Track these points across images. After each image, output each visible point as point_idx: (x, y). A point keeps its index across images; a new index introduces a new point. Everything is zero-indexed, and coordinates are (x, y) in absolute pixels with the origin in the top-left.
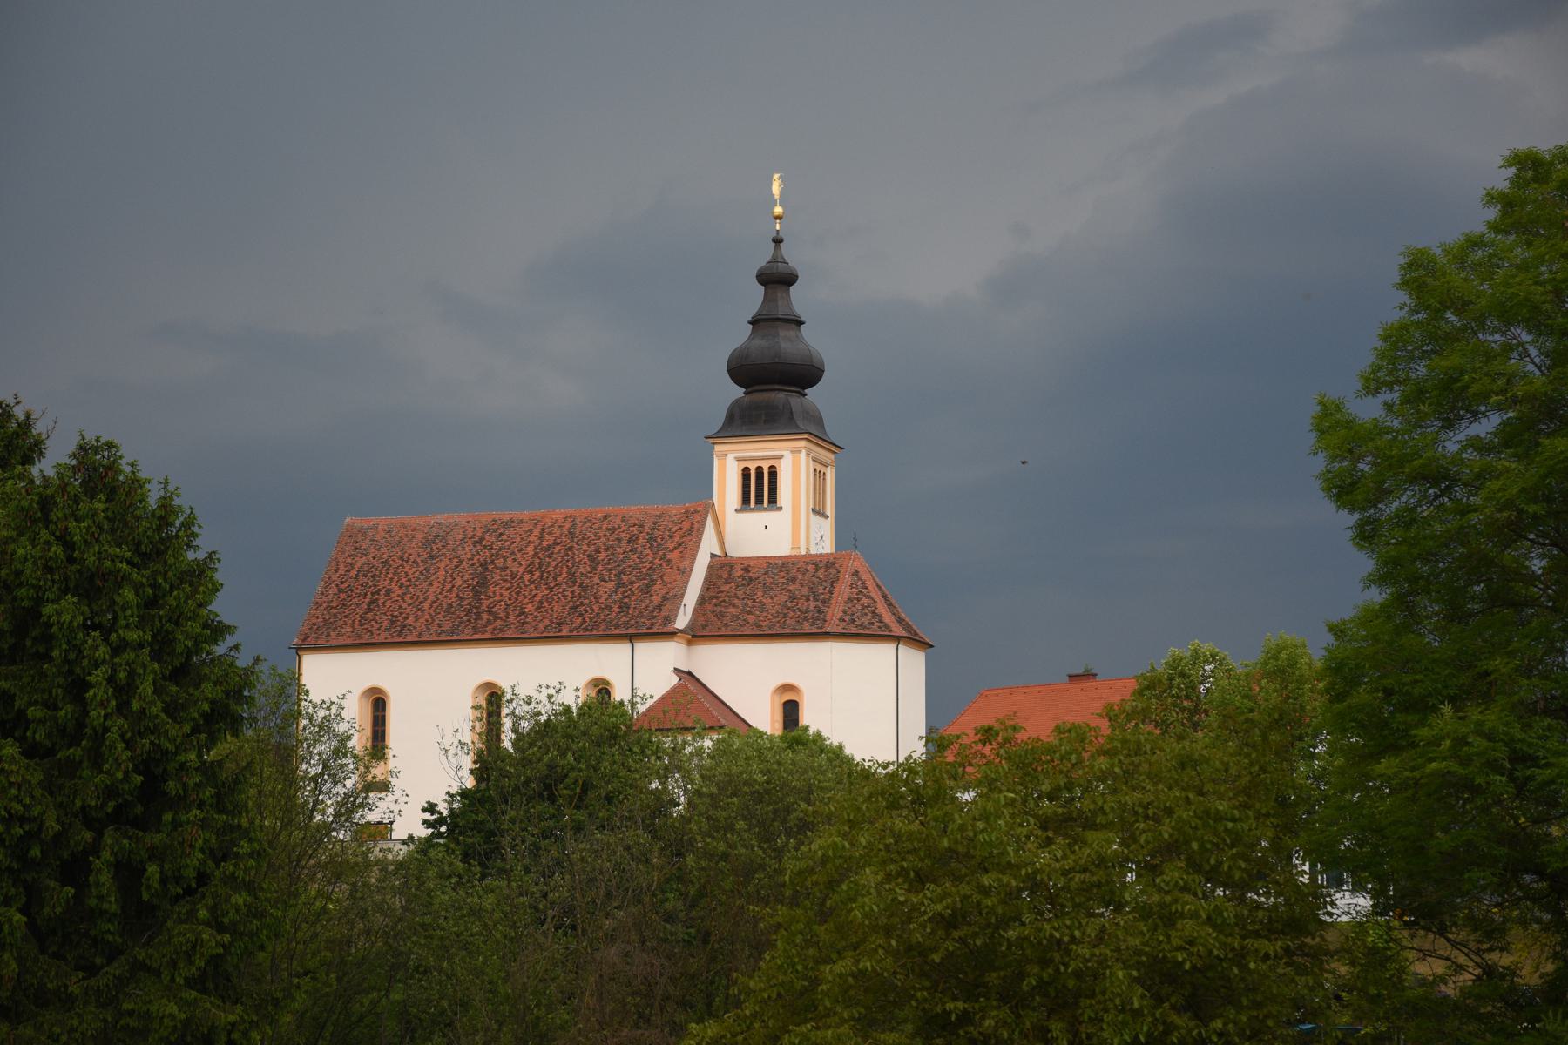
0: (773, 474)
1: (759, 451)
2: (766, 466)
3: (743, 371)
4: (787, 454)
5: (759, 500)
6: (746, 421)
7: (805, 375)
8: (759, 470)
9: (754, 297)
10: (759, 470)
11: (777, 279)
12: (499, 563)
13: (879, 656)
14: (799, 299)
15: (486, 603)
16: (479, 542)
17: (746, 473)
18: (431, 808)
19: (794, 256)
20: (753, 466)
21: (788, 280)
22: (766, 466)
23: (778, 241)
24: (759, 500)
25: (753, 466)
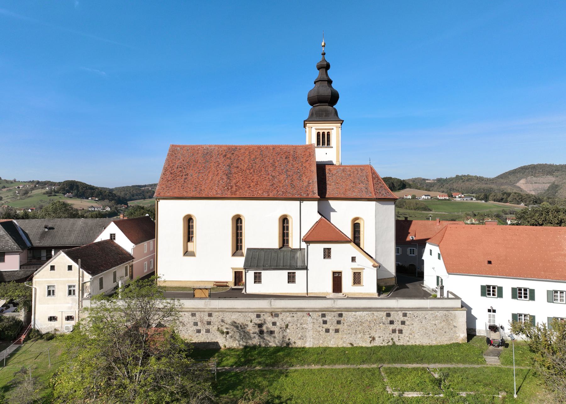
0: (328, 134)
1: (324, 127)
2: (326, 132)
3: (314, 101)
4: (335, 128)
5: (323, 144)
6: (315, 117)
7: (334, 98)
8: (323, 133)
9: (316, 74)
10: (323, 133)
11: (325, 67)
12: (235, 165)
13: (294, 248)
14: (331, 73)
15: (234, 181)
16: (225, 156)
17: (318, 134)
18: (334, 211)
19: (328, 59)
20: (321, 132)
21: (327, 67)
22: (326, 132)
23: (324, 54)
24: (323, 144)
25: (321, 132)
